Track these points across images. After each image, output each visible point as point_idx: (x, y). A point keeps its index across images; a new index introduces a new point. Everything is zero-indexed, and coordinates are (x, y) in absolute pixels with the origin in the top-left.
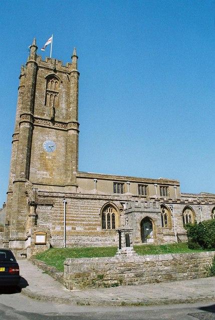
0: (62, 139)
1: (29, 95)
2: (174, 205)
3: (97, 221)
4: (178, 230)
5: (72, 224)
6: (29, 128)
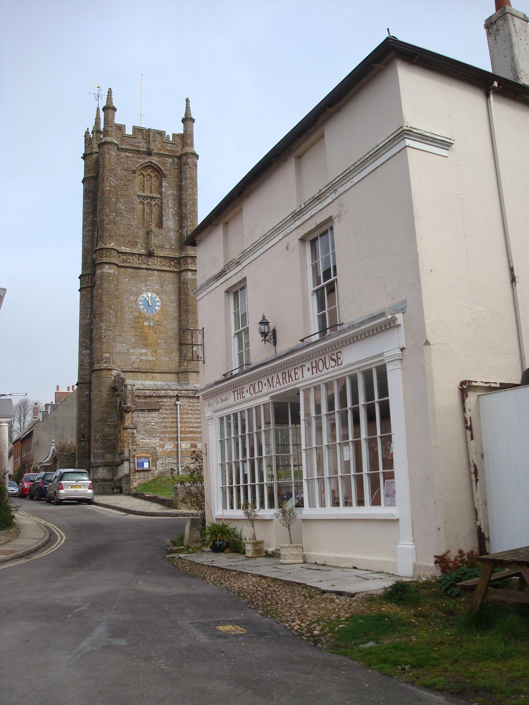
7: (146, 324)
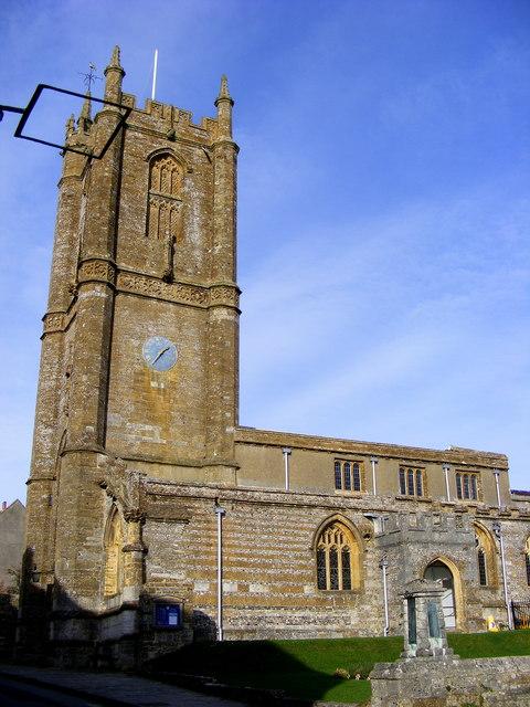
0: (192, 333)
1: (105, 206)
2: (506, 525)
3: (304, 567)
4: (515, 593)
5: (239, 575)
6: (107, 300)
7: (153, 384)
